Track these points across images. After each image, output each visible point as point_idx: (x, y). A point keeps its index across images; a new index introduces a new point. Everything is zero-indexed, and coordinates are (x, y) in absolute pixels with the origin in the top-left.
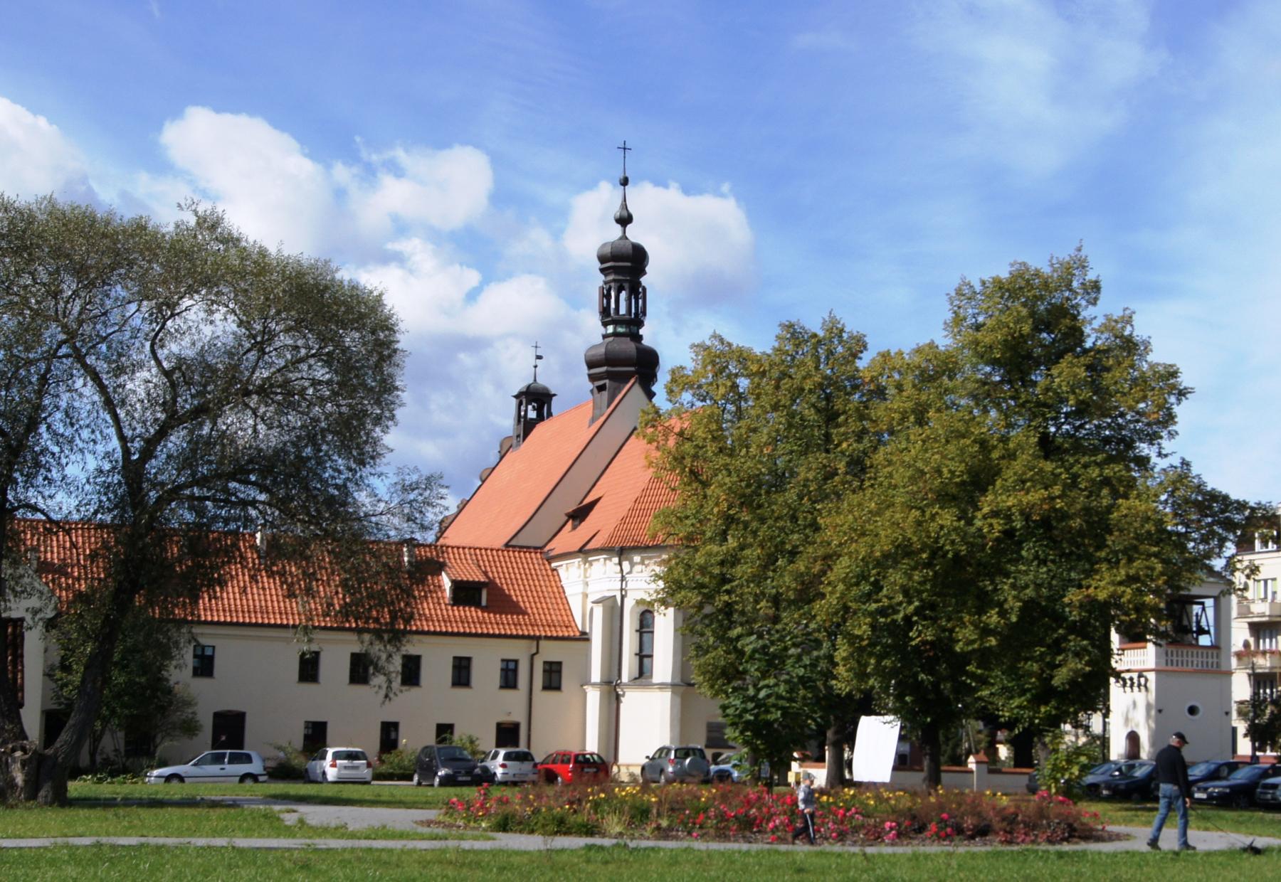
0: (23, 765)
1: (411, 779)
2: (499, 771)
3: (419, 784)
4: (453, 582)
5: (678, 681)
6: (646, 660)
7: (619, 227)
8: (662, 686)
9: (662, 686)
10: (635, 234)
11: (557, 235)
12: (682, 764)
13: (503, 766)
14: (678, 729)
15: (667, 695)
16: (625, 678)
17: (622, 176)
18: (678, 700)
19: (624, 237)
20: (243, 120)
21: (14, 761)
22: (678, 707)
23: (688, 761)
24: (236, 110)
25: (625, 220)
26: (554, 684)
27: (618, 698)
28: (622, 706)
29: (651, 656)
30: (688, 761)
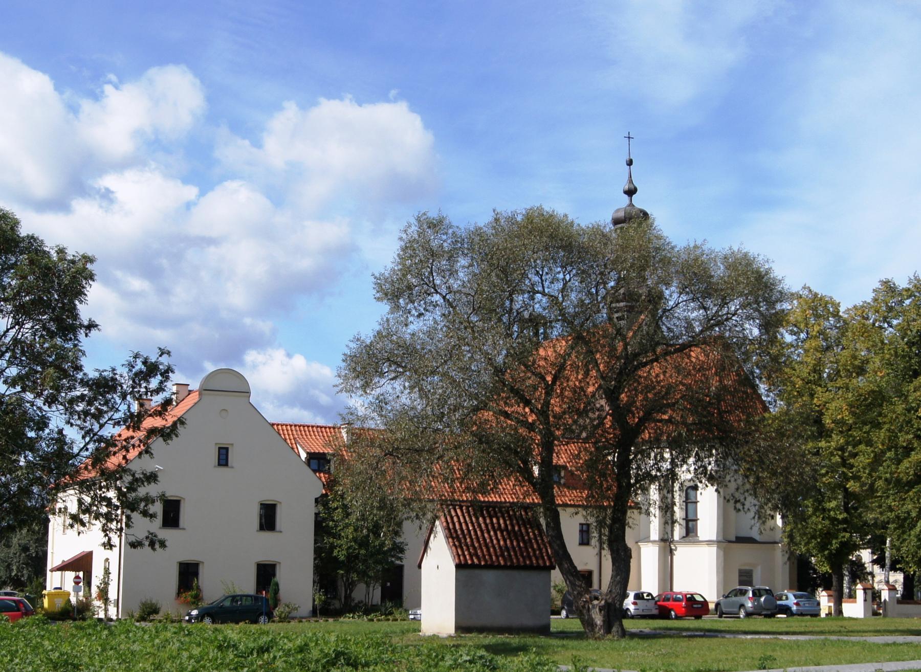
0: (600, 610)
1: (559, 614)
2: (632, 608)
3: (567, 617)
4: (308, 453)
5: (721, 538)
6: (691, 524)
7: (626, 196)
8: (709, 543)
9: (709, 543)
10: (639, 202)
11: (258, 144)
12: (759, 601)
13: (634, 603)
14: (721, 575)
15: (713, 549)
16: (677, 537)
17: (628, 158)
18: (722, 553)
19: (631, 205)
20: (40, 74)
21: (594, 607)
22: (722, 559)
23: (762, 599)
24: (35, 68)
25: (631, 192)
26: (585, 541)
27: (671, 552)
28: (675, 557)
29: (696, 520)
30: (762, 599)
